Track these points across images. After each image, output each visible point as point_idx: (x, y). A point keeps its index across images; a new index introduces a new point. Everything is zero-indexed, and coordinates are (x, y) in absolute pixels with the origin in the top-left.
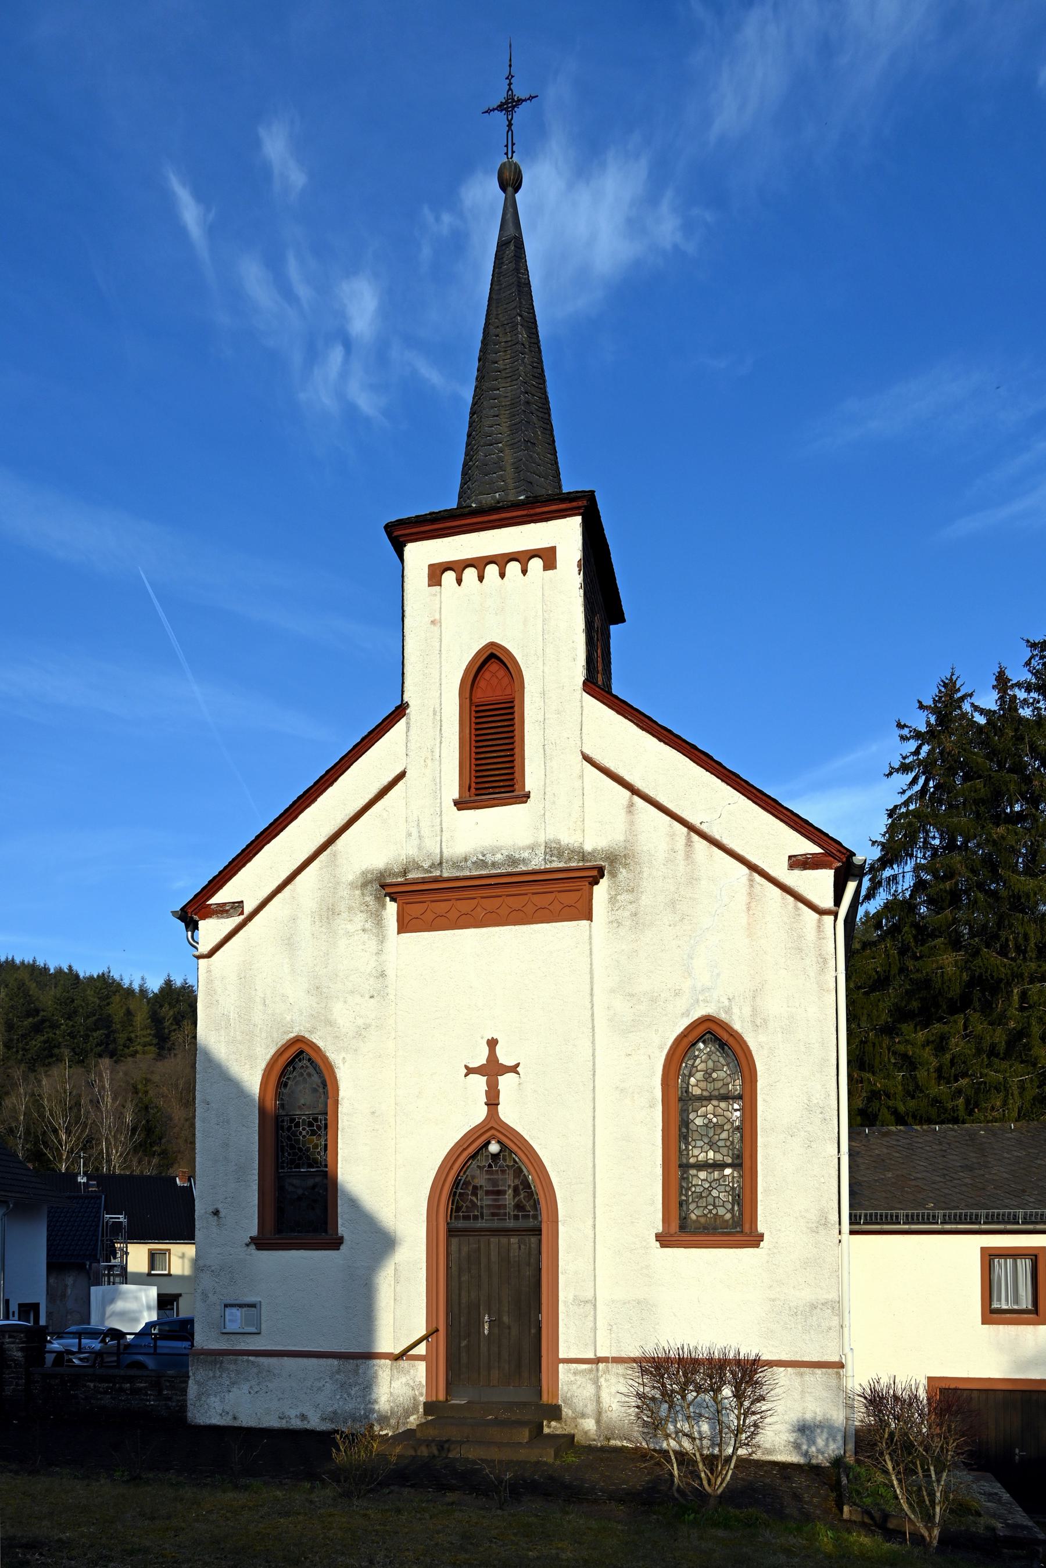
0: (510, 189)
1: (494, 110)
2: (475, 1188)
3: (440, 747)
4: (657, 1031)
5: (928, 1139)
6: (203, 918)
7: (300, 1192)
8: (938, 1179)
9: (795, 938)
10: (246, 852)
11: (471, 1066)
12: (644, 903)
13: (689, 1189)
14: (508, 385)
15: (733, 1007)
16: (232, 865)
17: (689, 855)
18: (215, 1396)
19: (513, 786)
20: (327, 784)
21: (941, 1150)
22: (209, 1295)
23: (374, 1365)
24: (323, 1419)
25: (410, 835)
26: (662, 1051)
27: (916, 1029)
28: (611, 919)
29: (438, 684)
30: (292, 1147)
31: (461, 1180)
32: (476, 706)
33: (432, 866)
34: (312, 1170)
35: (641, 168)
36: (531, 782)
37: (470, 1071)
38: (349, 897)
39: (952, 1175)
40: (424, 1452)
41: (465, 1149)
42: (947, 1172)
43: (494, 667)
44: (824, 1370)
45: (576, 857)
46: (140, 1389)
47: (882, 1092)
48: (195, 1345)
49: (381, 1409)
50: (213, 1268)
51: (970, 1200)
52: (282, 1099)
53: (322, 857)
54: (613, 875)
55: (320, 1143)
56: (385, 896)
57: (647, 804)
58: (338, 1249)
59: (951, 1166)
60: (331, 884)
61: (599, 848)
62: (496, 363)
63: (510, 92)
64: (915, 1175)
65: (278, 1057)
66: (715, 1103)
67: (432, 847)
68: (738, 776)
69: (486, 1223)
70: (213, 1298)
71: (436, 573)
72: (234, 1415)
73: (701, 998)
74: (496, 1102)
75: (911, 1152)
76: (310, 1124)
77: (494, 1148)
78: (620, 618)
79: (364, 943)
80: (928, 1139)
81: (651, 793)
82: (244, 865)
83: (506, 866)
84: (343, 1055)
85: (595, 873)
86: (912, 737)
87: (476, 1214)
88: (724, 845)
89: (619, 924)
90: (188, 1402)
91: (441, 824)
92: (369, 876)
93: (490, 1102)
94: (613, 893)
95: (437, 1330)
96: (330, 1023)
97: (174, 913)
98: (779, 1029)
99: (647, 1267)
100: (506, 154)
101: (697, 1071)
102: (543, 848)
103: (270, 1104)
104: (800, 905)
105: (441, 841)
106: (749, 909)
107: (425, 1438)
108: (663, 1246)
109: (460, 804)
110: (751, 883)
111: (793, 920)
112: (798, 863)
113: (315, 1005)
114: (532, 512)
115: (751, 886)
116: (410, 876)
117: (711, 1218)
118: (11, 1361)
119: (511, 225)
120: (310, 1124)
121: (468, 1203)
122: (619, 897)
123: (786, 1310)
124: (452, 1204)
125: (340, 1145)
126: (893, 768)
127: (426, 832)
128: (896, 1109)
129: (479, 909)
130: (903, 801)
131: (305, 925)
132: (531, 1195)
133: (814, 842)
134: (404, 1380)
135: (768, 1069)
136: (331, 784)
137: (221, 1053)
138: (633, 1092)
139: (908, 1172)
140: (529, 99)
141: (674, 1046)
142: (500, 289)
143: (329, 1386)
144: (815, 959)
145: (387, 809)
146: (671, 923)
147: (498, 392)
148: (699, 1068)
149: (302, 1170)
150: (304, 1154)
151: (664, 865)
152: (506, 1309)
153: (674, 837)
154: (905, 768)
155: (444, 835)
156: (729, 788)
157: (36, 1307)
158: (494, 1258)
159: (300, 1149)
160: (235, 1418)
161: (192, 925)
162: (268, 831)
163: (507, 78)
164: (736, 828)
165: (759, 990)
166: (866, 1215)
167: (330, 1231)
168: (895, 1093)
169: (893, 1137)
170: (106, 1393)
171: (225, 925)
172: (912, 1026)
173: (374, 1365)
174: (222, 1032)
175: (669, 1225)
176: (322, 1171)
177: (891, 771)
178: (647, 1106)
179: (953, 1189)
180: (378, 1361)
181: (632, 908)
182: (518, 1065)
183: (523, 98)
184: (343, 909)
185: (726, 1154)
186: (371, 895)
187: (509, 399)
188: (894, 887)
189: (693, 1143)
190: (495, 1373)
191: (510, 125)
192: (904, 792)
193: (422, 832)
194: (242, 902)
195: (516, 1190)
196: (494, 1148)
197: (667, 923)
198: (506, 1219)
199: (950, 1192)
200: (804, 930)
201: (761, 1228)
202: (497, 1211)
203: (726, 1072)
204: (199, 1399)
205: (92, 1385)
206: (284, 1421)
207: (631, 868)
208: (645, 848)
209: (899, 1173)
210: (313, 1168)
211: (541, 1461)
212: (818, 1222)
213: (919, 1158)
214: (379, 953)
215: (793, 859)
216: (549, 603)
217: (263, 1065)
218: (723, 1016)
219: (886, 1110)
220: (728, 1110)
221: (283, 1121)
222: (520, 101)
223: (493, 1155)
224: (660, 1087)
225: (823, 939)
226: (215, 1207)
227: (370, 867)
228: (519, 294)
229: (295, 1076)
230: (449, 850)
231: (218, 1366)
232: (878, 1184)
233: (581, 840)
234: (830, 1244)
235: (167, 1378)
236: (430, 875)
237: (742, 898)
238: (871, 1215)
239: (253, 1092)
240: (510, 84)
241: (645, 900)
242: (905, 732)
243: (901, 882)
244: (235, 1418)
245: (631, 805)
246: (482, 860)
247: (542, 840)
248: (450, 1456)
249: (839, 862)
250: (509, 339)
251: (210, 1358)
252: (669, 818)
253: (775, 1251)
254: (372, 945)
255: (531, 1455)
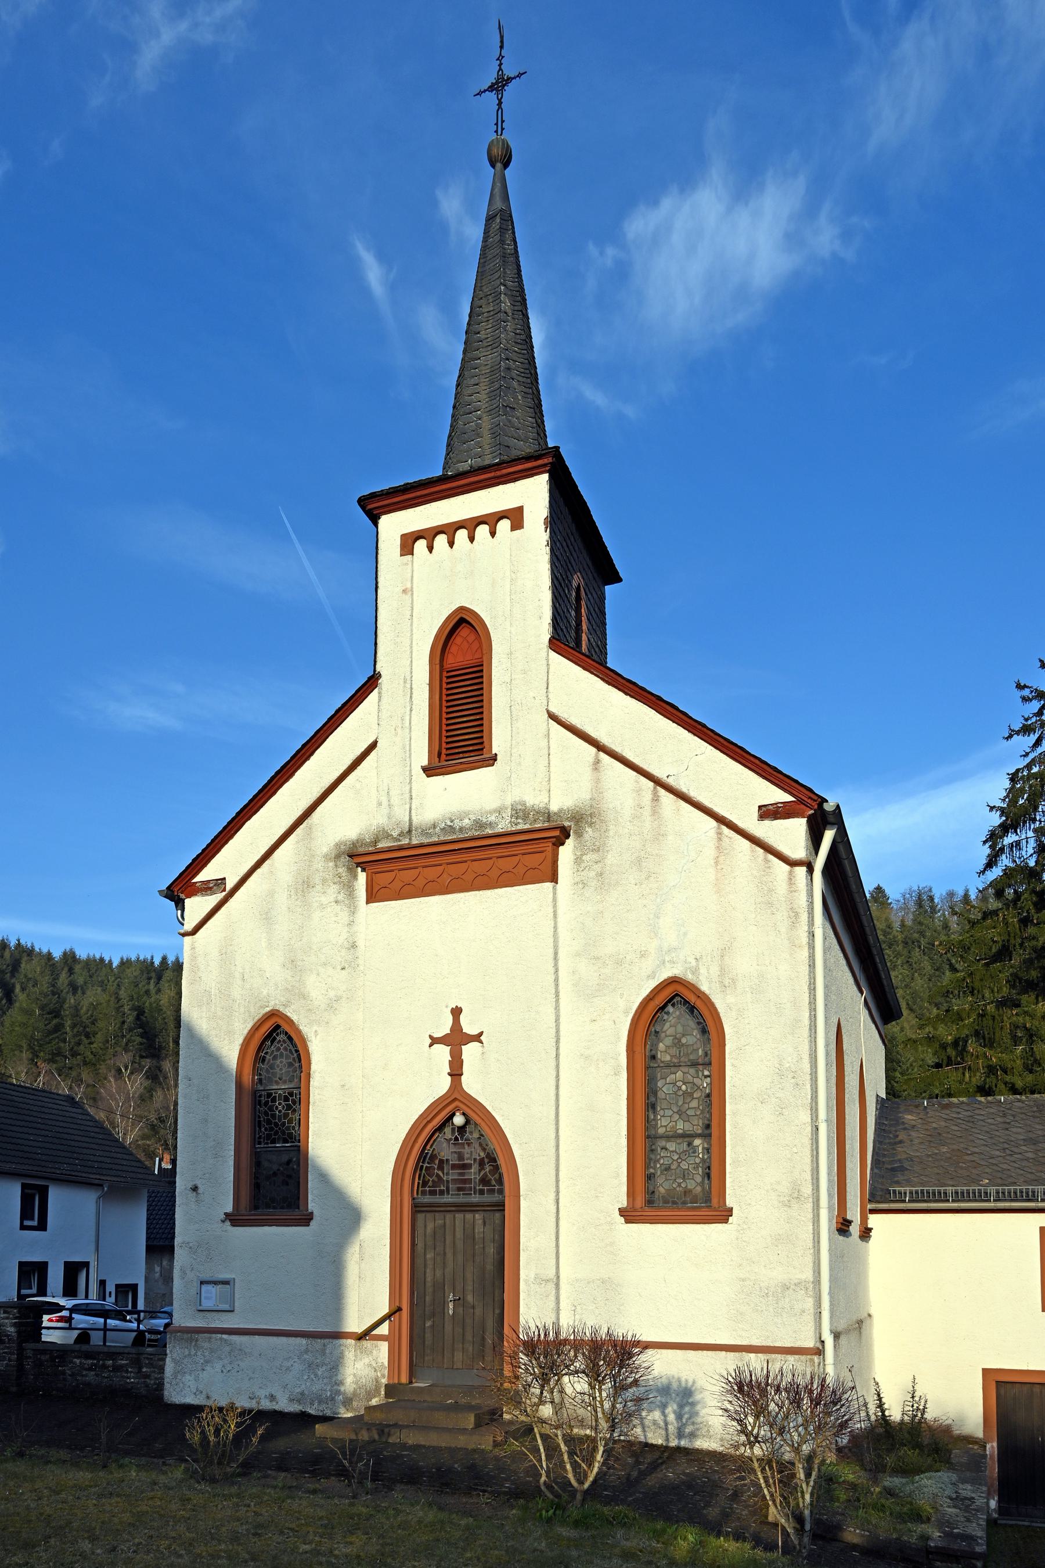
0: (499, 165)
1: (485, 91)
2: (441, 1161)
3: (410, 714)
4: (622, 995)
5: (992, 1110)
6: (189, 896)
7: (275, 1167)
8: (998, 1153)
9: (766, 892)
10: (228, 829)
11: (435, 1036)
12: (609, 862)
13: (658, 1161)
14: (488, 353)
15: (700, 967)
16: (215, 843)
17: (655, 812)
18: (190, 1374)
19: (482, 749)
20: (304, 759)
21: (1005, 1123)
22: (187, 1272)
23: (340, 1345)
24: (291, 1400)
25: (380, 804)
26: (627, 1016)
27: (1037, 1000)
28: (577, 880)
29: (408, 652)
30: (269, 1122)
31: (427, 1153)
32: (448, 672)
33: (401, 834)
34: (287, 1145)
35: (800, 184)
36: (498, 744)
37: (434, 1041)
38: (322, 868)
39: (1013, 1149)
40: (364, 1436)
41: (429, 1122)
42: (1007, 1146)
43: (464, 632)
44: (797, 1357)
45: (541, 818)
46: (122, 1366)
47: (998, 1067)
48: (173, 1322)
49: (347, 1391)
50: (191, 1245)
51: (1029, 1176)
52: (260, 1075)
53: (299, 831)
54: (579, 835)
55: (295, 1117)
56: (357, 867)
57: (612, 760)
58: (308, 1225)
59: (1013, 1139)
60: (306, 857)
61: (565, 808)
62: (479, 333)
63: (500, 73)
64: (972, 1149)
65: (255, 1031)
66: (685, 1069)
67: (402, 815)
68: (704, 726)
69: (451, 1198)
70: (191, 1275)
71: (408, 543)
72: (207, 1394)
73: (667, 959)
74: (460, 1073)
75: (971, 1124)
76: (286, 1099)
77: (459, 1120)
78: (615, 578)
79: (336, 915)
80: (992, 1110)
81: (618, 749)
82: (226, 842)
83: (473, 830)
84: (315, 1028)
85: (557, 833)
86: (1034, 698)
87: (442, 1188)
88: (690, 798)
89: (584, 885)
90: (165, 1380)
91: (411, 792)
92: (342, 847)
93: (454, 1073)
94: (579, 854)
95: (399, 1309)
96: (304, 996)
97: (160, 892)
98: (747, 989)
99: (612, 1244)
100: (496, 132)
101: (666, 1036)
102: (509, 810)
103: (247, 1079)
104: (771, 857)
105: (410, 808)
106: (717, 863)
107: (373, 1422)
108: (627, 1221)
109: (429, 771)
110: (720, 836)
111: (763, 873)
112: (768, 812)
113: (290, 979)
114: (498, 473)
115: (720, 839)
116: (380, 845)
117: (681, 1192)
118: (6, 1336)
119: (498, 198)
120: (286, 1099)
121: (434, 1177)
122: (584, 857)
123: (756, 1290)
124: (419, 1179)
125: (311, 1120)
126: (1013, 731)
127: (395, 800)
128: (1013, 1085)
129: (445, 875)
130: (1025, 764)
131: (282, 899)
132: (496, 1168)
133: (785, 790)
134: (366, 1361)
135: (737, 1032)
136: (308, 758)
137: (202, 1029)
138: (598, 1060)
139: (966, 1146)
140: (518, 76)
141: (640, 1010)
142: (485, 262)
143: (298, 1367)
144: (785, 913)
145: (360, 779)
146: (637, 882)
147: (479, 361)
148: (668, 1033)
149: (277, 1145)
150: (280, 1129)
151: (630, 821)
152: (470, 1288)
153: (640, 792)
154: (1026, 730)
155: (413, 803)
156: (696, 738)
157: (134, 1288)
158: (459, 1234)
159: (276, 1125)
160: (208, 1397)
161: (180, 904)
162: (248, 808)
163: (498, 59)
164: (704, 779)
165: (727, 948)
166: (911, 1193)
167: (301, 1208)
168: (1013, 1068)
169: (954, 1110)
170: (90, 1369)
171: (208, 902)
172: (1033, 997)
173: (340, 1345)
174: (204, 1008)
175: (634, 1200)
176: (296, 1146)
177: (1010, 734)
178: (612, 1074)
179: (1012, 1164)
180: (344, 1341)
181: (597, 868)
182: (481, 1034)
183: (513, 76)
184: (317, 882)
185: (696, 1123)
186: (344, 866)
187: (489, 367)
188: (1018, 853)
189: (662, 1113)
190: (459, 1356)
191: (500, 104)
192: (1027, 755)
193: (392, 801)
194: (225, 879)
195: (482, 1163)
196: (459, 1120)
197: (633, 882)
198: (471, 1194)
199: (1009, 1167)
200: (775, 883)
201: (730, 1202)
202: (463, 1186)
203: (695, 1037)
204: (176, 1377)
205: (78, 1361)
206: (254, 1401)
207: (597, 826)
208: (611, 806)
209: (955, 1147)
210: (288, 1143)
211: (479, 1449)
212: (791, 1195)
213: (979, 1132)
214: (351, 924)
215: (763, 808)
216: (515, 563)
217: (240, 1040)
218: (690, 977)
219: (1004, 1086)
220: (698, 1077)
221: (260, 1096)
222: (510, 79)
223: (459, 1128)
224: (625, 1053)
225: (795, 891)
226: (194, 1183)
227: (344, 839)
228: (503, 265)
229: (273, 1051)
230: (418, 817)
231: (193, 1344)
232: (930, 1159)
233: (546, 800)
234: (803, 1219)
235: (146, 1356)
236: (399, 843)
237: (710, 852)
238: (917, 1192)
239: (231, 1067)
240: (500, 65)
241: (611, 859)
242: (1026, 692)
243: (1024, 848)
244: (208, 1397)
245: (597, 761)
246: (450, 826)
247: (509, 801)
248: (390, 1441)
249: (812, 809)
250: (492, 309)
251: (186, 1336)
252: (635, 773)
253: (745, 1227)
254: (344, 916)
255: (485, 1442)
